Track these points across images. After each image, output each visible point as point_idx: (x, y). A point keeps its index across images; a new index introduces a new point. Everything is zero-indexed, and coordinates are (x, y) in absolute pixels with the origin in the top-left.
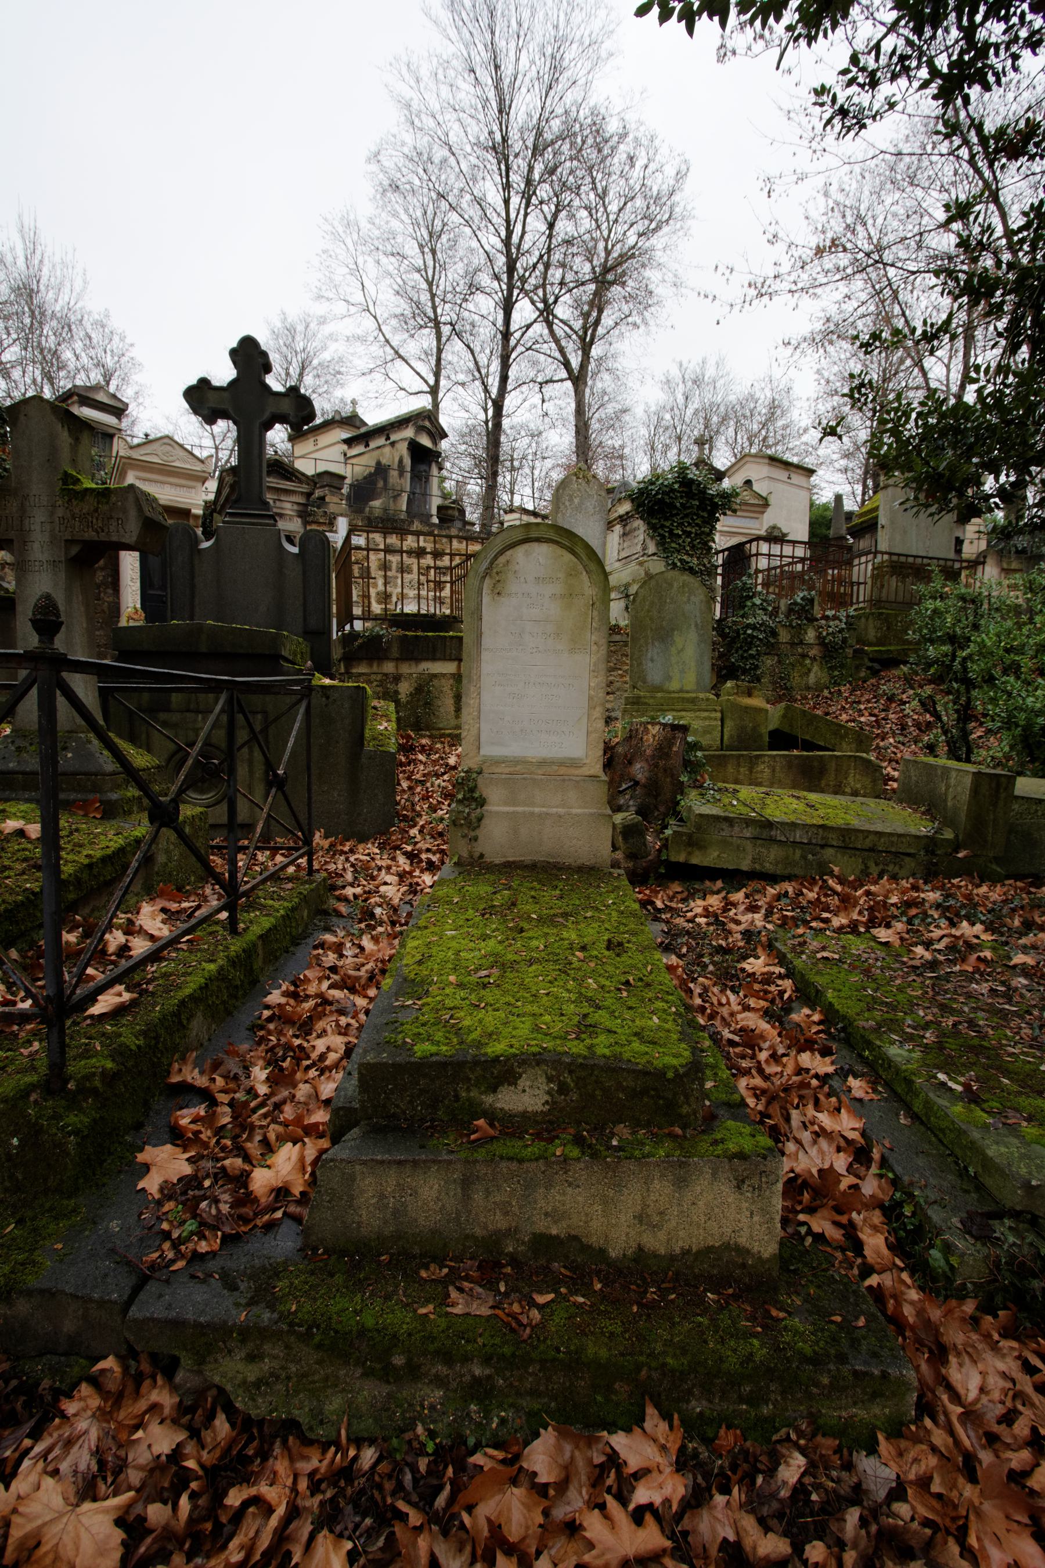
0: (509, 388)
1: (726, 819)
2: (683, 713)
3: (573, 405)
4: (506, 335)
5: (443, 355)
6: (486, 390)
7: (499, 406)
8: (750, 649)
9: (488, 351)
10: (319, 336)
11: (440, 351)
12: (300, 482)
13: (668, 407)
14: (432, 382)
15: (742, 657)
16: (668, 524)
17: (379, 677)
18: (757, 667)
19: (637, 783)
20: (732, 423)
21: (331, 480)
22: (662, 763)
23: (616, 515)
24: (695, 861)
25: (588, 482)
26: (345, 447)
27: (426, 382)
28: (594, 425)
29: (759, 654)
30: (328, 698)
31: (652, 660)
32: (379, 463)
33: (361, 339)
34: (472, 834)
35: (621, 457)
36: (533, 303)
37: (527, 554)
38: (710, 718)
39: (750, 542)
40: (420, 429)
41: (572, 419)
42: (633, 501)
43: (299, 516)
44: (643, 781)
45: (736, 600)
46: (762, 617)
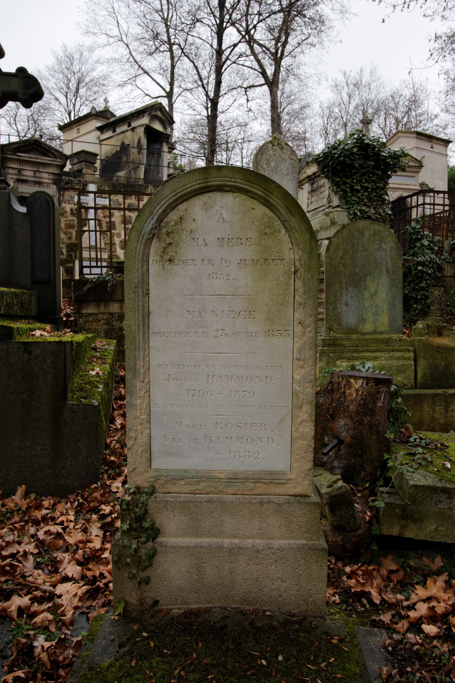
0: (222, 92)
1: (444, 490)
2: (378, 354)
3: (269, 104)
4: (220, 52)
5: (176, 71)
6: (207, 95)
7: (214, 102)
8: (421, 282)
9: (208, 69)
10: (90, 61)
11: (173, 67)
12: (55, 157)
13: (337, 104)
14: (168, 89)
15: (414, 289)
16: (349, 181)
17: (106, 316)
18: (427, 297)
19: (341, 442)
20: (382, 113)
21: (86, 157)
22: (366, 420)
23: (305, 175)
24: (409, 534)
25: (282, 148)
26: (99, 133)
27: (164, 89)
28: (285, 117)
29: (428, 286)
30: (30, 354)
31: (347, 305)
32: (123, 143)
33: (118, 61)
34: (143, 575)
35: (304, 139)
36: (239, 31)
37: (207, 208)
38: (404, 358)
39: (411, 196)
40: (154, 118)
41: (269, 113)
42: (319, 163)
43: (55, 184)
44: (348, 440)
45: (408, 242)
46: (430, 256)
